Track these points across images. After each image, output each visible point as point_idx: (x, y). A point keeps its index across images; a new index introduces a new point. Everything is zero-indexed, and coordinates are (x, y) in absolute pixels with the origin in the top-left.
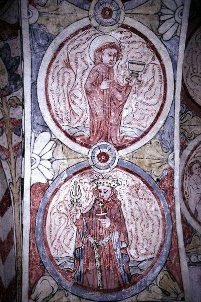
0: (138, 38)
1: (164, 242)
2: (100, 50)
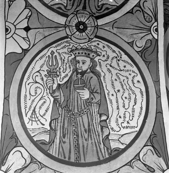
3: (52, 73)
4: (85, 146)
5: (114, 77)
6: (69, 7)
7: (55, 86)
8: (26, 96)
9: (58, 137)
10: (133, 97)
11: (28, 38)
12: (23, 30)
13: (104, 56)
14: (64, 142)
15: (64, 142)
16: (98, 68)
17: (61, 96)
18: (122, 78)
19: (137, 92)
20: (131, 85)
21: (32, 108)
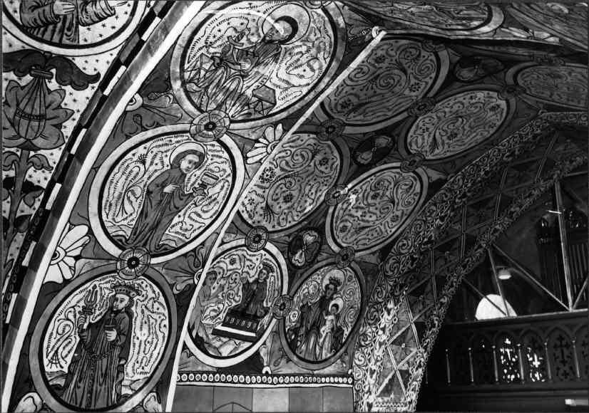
0: (226, 155)
1: (153, 229)
2: (182, 156)
3: (87, 310)
4: (99, 390)
5: (145, 319)
6: (130, 241)
7: (85, 326)
8: (52, 333)
9: (74, 381)
10: (155, 341)
11: (75, 267)
12: (72, 258)
13: (143, 296)
14: (79, 387)
15: (79, 387)
16: (133, 309)
17: (88, 336)
18: (152, 320)
19: (160, 336)
20: (157, 328)
21: (55, 349)
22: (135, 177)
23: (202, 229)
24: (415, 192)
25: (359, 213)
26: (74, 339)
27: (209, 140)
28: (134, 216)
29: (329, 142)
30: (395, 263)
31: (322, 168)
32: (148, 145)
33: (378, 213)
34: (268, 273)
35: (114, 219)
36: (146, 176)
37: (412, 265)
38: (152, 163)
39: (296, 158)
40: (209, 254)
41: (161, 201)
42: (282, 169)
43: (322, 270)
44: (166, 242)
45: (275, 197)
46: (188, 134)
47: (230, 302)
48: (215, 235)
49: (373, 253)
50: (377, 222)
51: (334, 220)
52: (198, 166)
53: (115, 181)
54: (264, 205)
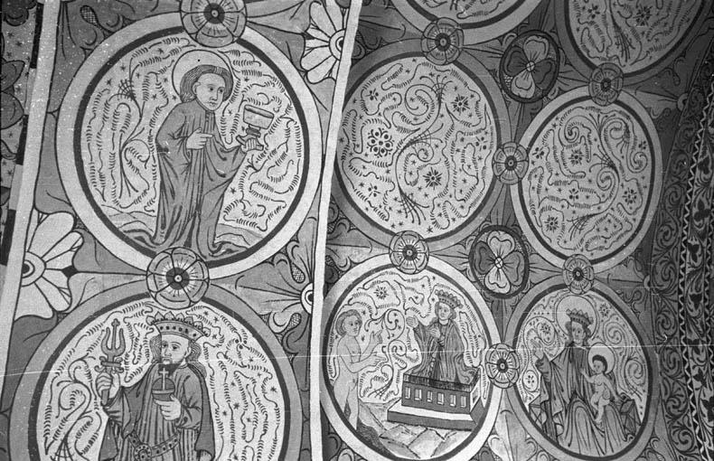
0: (265, 68)
3: (111, 363)
6: (159, 239)
8: (49, 409)
10: (261, 417)
11: (69, 289)
12: (60, 272)
17: (121, 409)
19: (270, 409)
21: (62, 437)
22: (127, 123)
23: (283, 212)
24: (639, 143)
25: (565, 193)
26: (96, 418)
27: (224, 41)
28: (151, 193)
29: (452, 66)
30: (667, 265)
31: (464, 116)
32: (124, 60)
33: (595, 188)
34: (453, 308)
35: (116, 202)
36: (146, 121)
37: (695, 259)
38: (146, 97)
39: (413, 105)
40: (313, 255)
41: (189, 164)
42: (400, 129)
43: (547, 297)
44: (226, 239)
45: (410, 179)
46: (184, 35)
47: (402, 361)
48: (311, 224)
49: (625, 262)
50: (604, 207)
51: (528, 208)
52: (228, 93)
53: (94, 133)
54: (396, 193)
